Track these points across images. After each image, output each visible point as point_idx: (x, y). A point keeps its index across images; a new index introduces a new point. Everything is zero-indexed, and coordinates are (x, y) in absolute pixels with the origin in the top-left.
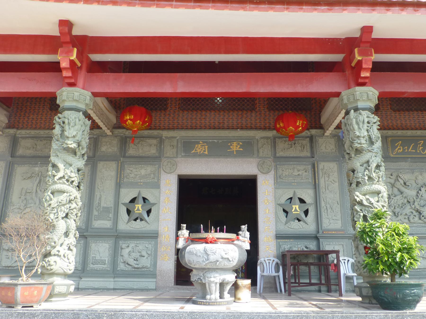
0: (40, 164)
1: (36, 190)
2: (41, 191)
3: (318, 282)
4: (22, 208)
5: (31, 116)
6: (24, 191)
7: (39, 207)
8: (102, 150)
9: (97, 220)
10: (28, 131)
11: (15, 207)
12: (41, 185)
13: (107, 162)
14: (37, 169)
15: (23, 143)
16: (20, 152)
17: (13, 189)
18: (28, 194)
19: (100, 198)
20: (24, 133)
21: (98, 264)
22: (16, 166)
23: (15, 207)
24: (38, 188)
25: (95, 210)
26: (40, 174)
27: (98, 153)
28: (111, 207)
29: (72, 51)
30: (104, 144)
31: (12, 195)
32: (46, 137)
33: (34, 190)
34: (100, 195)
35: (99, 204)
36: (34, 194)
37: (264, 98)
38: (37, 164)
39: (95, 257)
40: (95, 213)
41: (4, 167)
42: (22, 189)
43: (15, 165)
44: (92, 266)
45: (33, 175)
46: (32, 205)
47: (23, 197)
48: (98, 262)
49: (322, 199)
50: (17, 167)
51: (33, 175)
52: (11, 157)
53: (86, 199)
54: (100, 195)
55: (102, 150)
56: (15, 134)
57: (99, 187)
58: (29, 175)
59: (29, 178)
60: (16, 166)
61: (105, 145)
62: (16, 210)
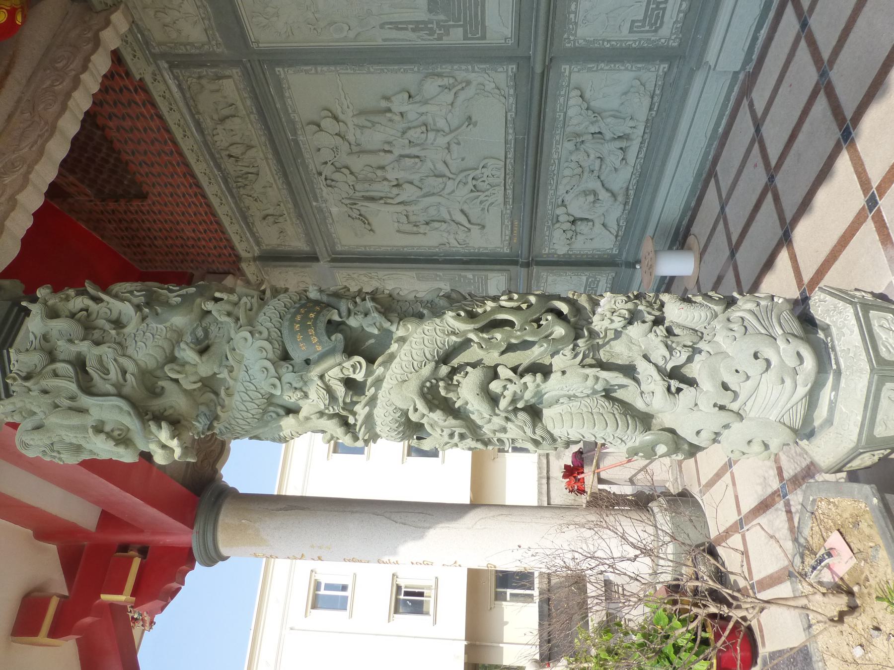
0: (317, 201)
1: (398, 203)
5: (190, 234)
8: (204, 39)
9: (484, 27)
10: (235, 239)
12: (382, 195)
13: (244, 14)
14: (334, 210)
15: (271, 238)
16: (296, 242)
19: (397, 26)
20: (236, 227)
21: (664, 9)
24: (389, 201)
25: (446, 41)
27: (218, 51)
28: (484, 37)
29: (112, 605)
30: (174, 35)
31: (413, 247)
32: (233, 196)
33: (400, 208)
34: (382, 26)
35: (418, 26)
37: (669, 389)
38: (320, 210)
39: (633, 22)
40: (456, 37)
42: (399, 231)
44: (666, 31)
47: (423, 229)
48: (658, 8)
50: (342, 246)
53: (405, 71)
54: (382, 26)
55: (204, 39)
56: (255, 259)
57: (352, 35)
61: (179, 31)
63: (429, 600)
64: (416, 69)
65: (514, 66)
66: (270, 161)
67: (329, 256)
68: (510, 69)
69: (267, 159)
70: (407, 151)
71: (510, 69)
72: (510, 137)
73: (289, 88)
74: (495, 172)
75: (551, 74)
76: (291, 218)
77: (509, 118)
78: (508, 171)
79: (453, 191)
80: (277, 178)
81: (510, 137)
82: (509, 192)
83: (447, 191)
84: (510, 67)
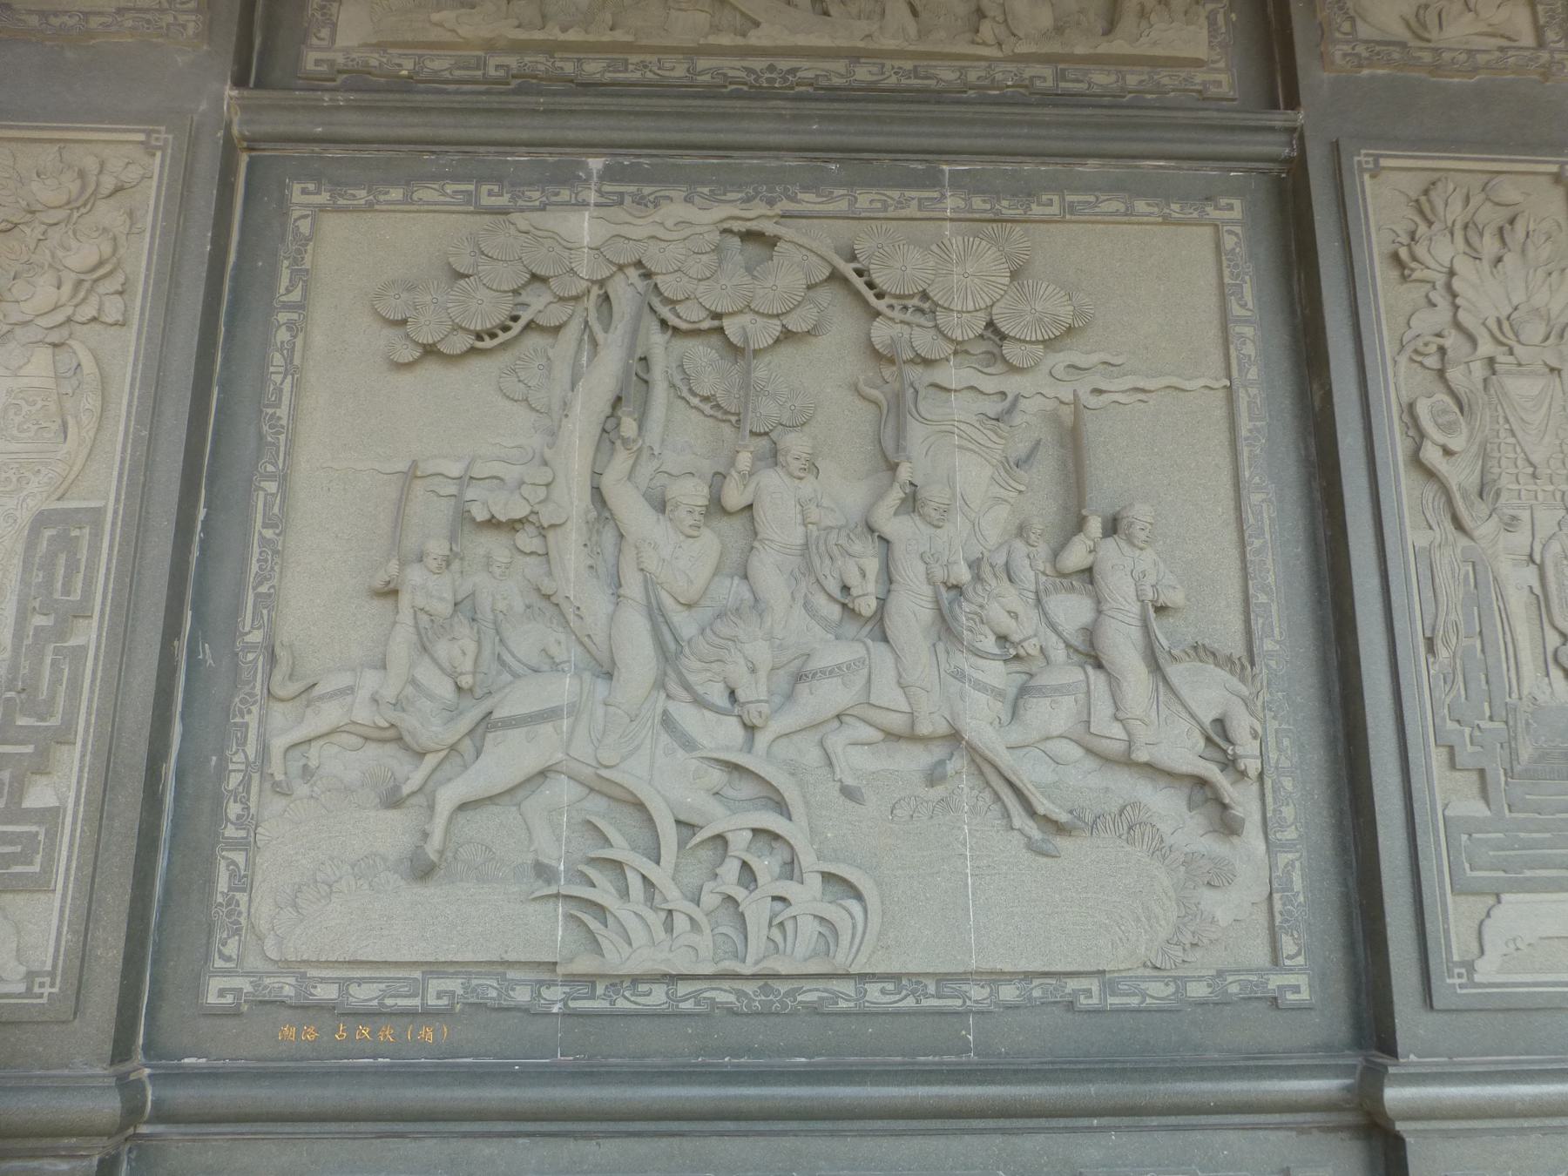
0: (608, 174)
2: (661, 505)
3: (1518, 768)
4: (432, 729)
6: (430, 516)
7: (667, 721)
11: (331, 714)
17: (284, 479)
18: (494, 545)
22: (301, 195)
23: (331, 714)
26: (625, 291)
28: (95, 517)
31: (278, 522)
33: (573, 500)
36: (571, 549)
38: (567, 176)
41: (150, 196)
42: (411, 475)
43: (296, 192)
45: (537, 304)
46: (564, 689)
49: (1394, 444)
51: (537, 304)
52: (240, 81)
57: (1432, 455)
58: (486, 309)
59: (485, 341)
60: (301, 195)
62: (344, 763)
63: (1110, 512)
64: (272, 487)
65: (1305, 995)
66: (840, 66)
67: (252, 143)
68: (1291, 979)
69: (855, 56)
70: (911, 572)
71: (1291, 979)
72: (977, 993)
73: (1167, 221)
74: (794, 934)
75: (1273, 1136)
76: (517, 47)
77: (1072, 984)
78: (783, 987)
79: (689, 744)
80: (759, 64)
81: (977, 993)
82: (657, 996)
83: (688, 716)
84: (1302, 980)
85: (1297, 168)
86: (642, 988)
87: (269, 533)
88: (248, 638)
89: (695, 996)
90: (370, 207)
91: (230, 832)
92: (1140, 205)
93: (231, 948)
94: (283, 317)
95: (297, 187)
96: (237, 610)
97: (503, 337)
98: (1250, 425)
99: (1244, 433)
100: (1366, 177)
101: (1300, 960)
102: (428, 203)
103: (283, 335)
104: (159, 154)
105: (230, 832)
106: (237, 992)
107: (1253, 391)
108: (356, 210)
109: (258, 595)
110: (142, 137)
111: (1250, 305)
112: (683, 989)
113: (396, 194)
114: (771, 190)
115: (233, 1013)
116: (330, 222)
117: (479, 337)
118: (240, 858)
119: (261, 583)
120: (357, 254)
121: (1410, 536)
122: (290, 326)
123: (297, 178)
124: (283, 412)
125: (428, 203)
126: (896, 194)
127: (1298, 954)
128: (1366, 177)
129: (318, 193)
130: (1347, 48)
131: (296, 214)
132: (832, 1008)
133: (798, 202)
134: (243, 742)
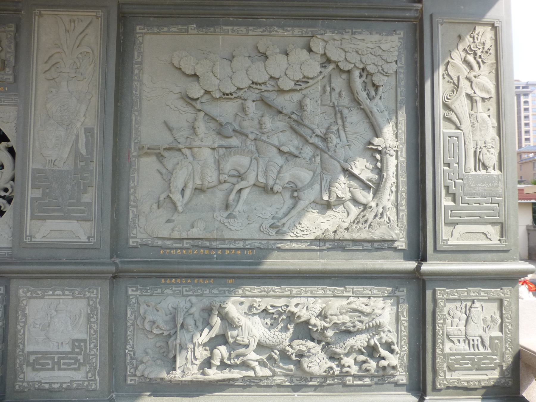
22: (138, 29)
64: (136, 113)
85: (421, 20)
86: (237, 242)
87: (137, 126)
88: (133, 154)
89: (250, 244)
90: (158, 33)
91: (132, 203)
92: (47, 386)
93: (135, 232)
94: (136, 66)
95: (138, 27)
96: (130, 146)
97: (230, 96)
98: (134, 175)
99: (399, 100)
100: (440, 25)
101: (403, 239)
102: (174, 32)
103: (136, 71)
104: (100, 19)
105: (132, 203)
106: (137, 242)
107: (402, 88)
108: (154, 34)
109: (135, 143)
110: (94, 14)
111: (403, 63)
112: (247, 242)
113: (166, 29)
114: (270, 28)
115: (135, 248)
116: (147, 37)
117: (224, 94)
118: (135, 210)
119: (135, 140)
120: (158, 49)
121: (442, 130)
122: (138, 68)
123: (138, 25)
124: (138, 93)
125: (174, 32)
126: (305, 30)
127: (403, 238)
128: (440, 25)
129: (144, 29)
130: (21, 384)
131: (138, 35)
132: (284, 384)
133: (277, 32)
134: (134, 181)
